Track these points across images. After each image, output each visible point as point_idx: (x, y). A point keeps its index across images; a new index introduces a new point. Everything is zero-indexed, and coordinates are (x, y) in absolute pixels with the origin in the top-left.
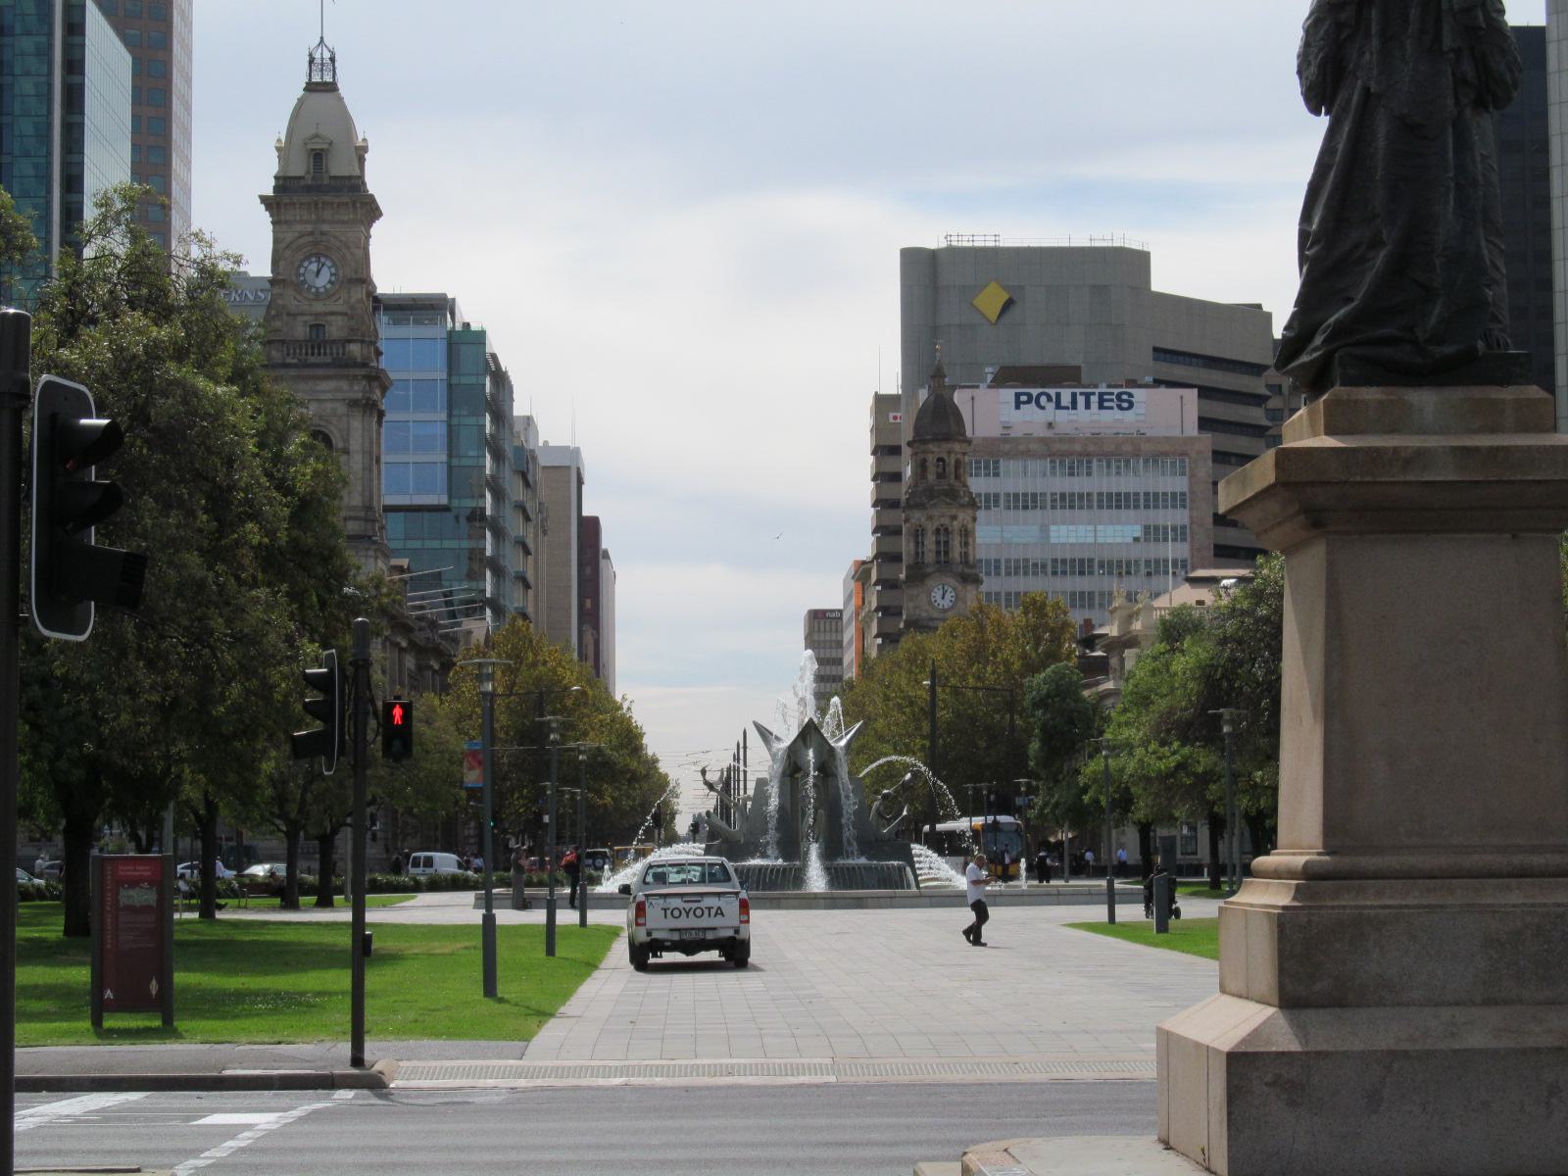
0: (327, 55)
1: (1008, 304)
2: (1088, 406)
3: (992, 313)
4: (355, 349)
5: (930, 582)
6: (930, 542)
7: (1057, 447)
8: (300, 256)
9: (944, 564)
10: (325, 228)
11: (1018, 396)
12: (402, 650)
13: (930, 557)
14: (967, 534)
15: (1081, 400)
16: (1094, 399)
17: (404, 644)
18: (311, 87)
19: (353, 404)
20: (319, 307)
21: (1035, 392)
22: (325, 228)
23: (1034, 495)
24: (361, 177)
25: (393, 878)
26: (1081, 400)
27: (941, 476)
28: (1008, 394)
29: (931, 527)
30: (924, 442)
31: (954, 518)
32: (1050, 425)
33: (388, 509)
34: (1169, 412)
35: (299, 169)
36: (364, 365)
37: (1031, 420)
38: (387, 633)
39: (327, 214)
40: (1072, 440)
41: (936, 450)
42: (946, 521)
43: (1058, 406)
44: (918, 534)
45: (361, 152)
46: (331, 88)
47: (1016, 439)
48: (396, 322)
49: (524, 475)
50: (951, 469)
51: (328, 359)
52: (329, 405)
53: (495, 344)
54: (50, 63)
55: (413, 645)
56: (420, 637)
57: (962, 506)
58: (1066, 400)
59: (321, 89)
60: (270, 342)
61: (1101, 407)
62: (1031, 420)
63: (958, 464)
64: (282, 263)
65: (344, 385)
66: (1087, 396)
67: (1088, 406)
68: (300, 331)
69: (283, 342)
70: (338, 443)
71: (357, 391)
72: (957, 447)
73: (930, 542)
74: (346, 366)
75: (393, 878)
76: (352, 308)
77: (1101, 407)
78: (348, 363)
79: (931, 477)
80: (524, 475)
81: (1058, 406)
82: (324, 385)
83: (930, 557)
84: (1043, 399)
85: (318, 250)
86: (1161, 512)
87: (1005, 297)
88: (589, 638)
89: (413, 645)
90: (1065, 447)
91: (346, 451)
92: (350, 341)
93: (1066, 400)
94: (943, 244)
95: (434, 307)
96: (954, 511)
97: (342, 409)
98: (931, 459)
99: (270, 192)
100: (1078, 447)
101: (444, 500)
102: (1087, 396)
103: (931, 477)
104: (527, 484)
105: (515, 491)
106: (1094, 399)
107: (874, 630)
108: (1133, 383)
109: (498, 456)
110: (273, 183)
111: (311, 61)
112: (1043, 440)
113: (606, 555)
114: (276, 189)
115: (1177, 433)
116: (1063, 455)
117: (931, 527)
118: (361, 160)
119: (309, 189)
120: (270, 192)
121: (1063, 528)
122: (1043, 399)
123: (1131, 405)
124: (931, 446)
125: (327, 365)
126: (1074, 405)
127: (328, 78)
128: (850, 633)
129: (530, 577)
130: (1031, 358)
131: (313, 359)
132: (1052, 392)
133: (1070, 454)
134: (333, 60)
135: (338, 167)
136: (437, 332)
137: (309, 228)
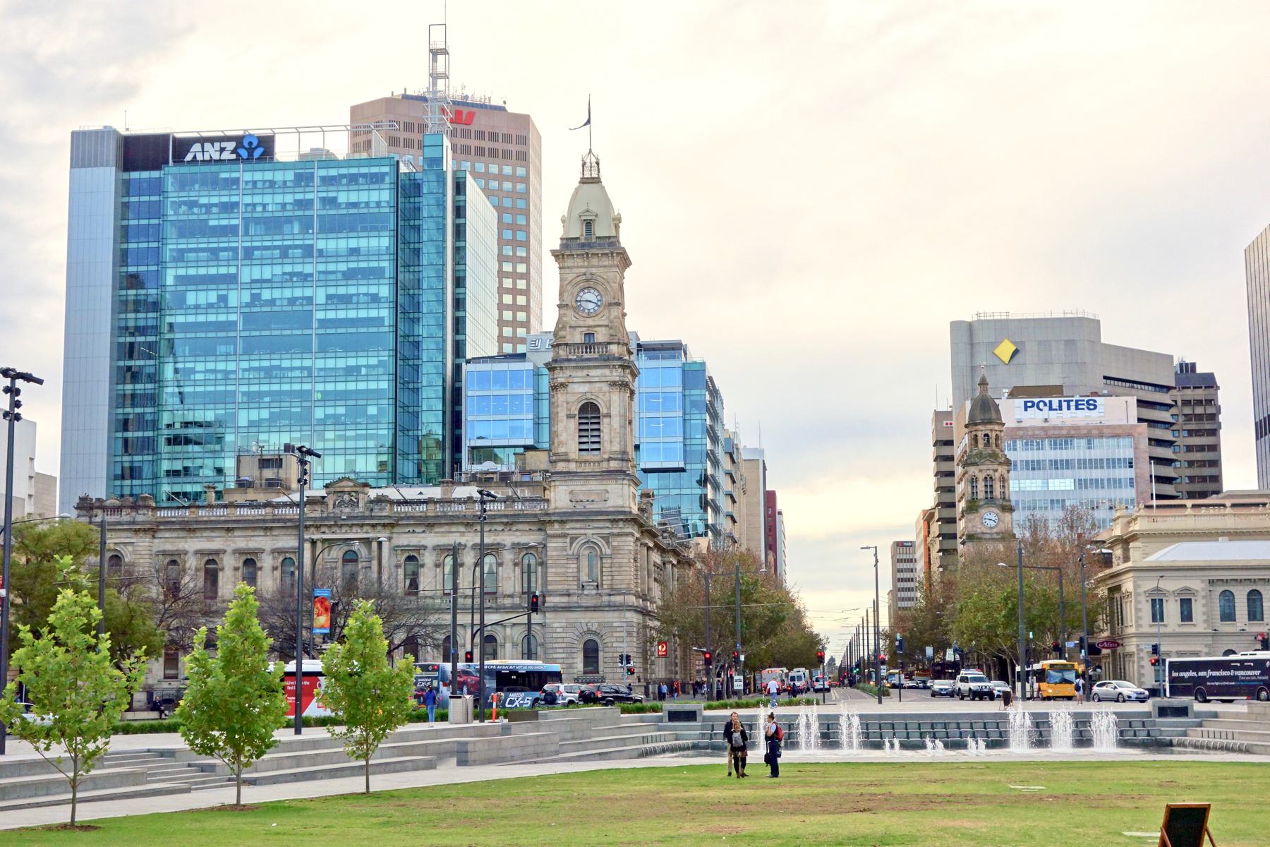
0: (594, 160)
1: (1015, 353)
2: (1069, 408)
3: (1006, 358)
4: (614, 349)
5: (982, 511)
6: (981, 486)
7: (1051, 432)
8: (577, 289)
9: (990, 500)
10: (594, 270)
11: (1026, 403)
12: (649, 548)
13: (981, 495)
14: (1003, 480)
15: (1064, 405)
16: (1073, 404)
17: (651, 545)
18: (584, 181)
19: (613, 384)
20: (590, 322)
21: (1036, 400)
22: (594, 270)
23: (1038, 462)
24: (617, 237)
25: (1108, 571)
26: (1064, 405)
27: (987, 444)
28: (1020, 402)
29: (981, 476)
30: (976, 424)
31: (996, 471)
32: (1046, 420)
33: (646, 471)
34: (1119, 410)
35: (577, 231)
36: (620, 359)
37: (1034, 418)
38: (637, 535)
39: (595, 261)
40: (1061, 428)
41: (982, 430)
42: (991, 473)
43: (1051, 409)
44: (973, 481)
45: (617, 221)
46: (597, 181)
47: (1025, 428)
48: (651, 358)
49: (731, 455)
50: (993, 441)
51: (596, 355)
52: (598, 385)
53: (711, 371)
54: (445, 208)
55: (656, 545)
56: (664, 542)
57: (1000, 464)
58: (1055, 405)
59: (591, 181)
60: (558, 345)
61: (1077, 408)
62: (1034, 418)
63: (997, 437)
64: (566, 295)
65: (607, 372)
66: (1068, 402)
67: (1069, 408)
68: (578, 338)
69: (567, 345)
70: (603, 410)
71: (616, 375)
72: (996, 427)
73: (981, 486)
74: (608, 359)
75: (1108, 571)
76: (611, 322)
77: (1077, 408)
78: (610, 358)
79: (981, 446)
80: (731, 455)
81: (1051, 409)
82: (593, 372)
83: (981, 495)
84: (1041, 405)
85: (589, 282)
86: (1117, 470)
87: (1013, 348)
88: (771, 558)
89: (656, 545)
90: (1056, 432)
91: (608, 415)
92: (609, 343)
93: (1055, 405)
94: (975, 318)
95: (674, 349)
96: (995, 467)
97: (605, 387)
98: (980, 435)
99: (558, 247)
100: (1064, 432)
101: (681, 465)
102: (1068, 402)
103: (981, 446)
104: (733, 461)
105: (726, 463)
106: (1073, 404)
107: (937, 547)
108: (1095, 394)
109: (715, 440)
110: (559, 242)
111: (584, 165)
112: (1042, 428)
113: (780, 513)
114: (562, 245)
115: (1124, 422)
116: (1056, 437)
117: (981, 476)
118: (617, 227)
119: (583, 245)
120: (558, 247)
121: (1057, 481)
122: (1041, 405)
123: (1095, 407)
124: (980, 427)
125: (596, 359)
126: (1060, 408)
127: (595, 175)
128: (920, 552)
129: (736, 537)
130: (1030, 381)
131: (586, 356)
132: (1047, 400)
133: (1060, 437)
134: (598, 163)
135: (600, 230)
136: (677, 363)
137: (583, 270)
